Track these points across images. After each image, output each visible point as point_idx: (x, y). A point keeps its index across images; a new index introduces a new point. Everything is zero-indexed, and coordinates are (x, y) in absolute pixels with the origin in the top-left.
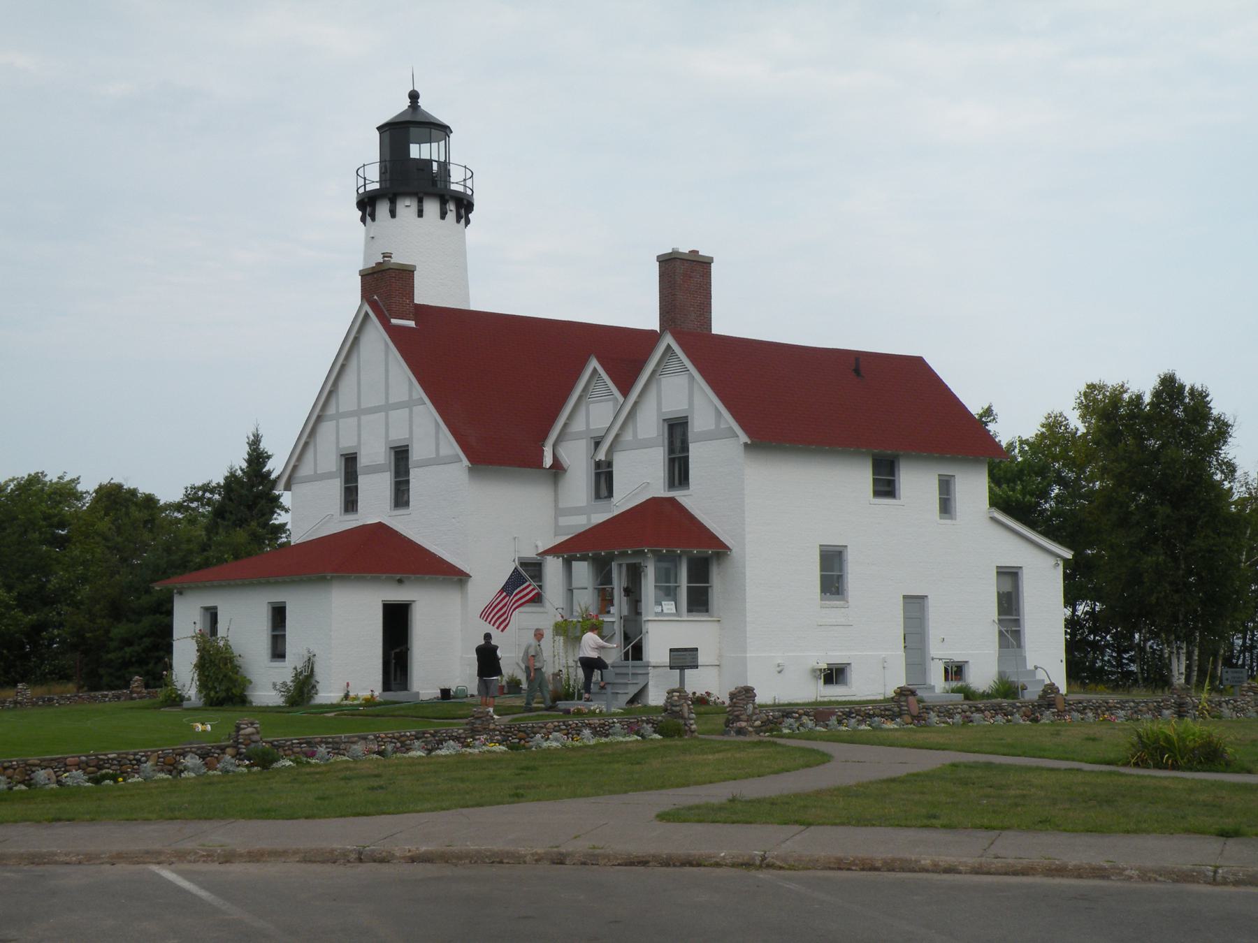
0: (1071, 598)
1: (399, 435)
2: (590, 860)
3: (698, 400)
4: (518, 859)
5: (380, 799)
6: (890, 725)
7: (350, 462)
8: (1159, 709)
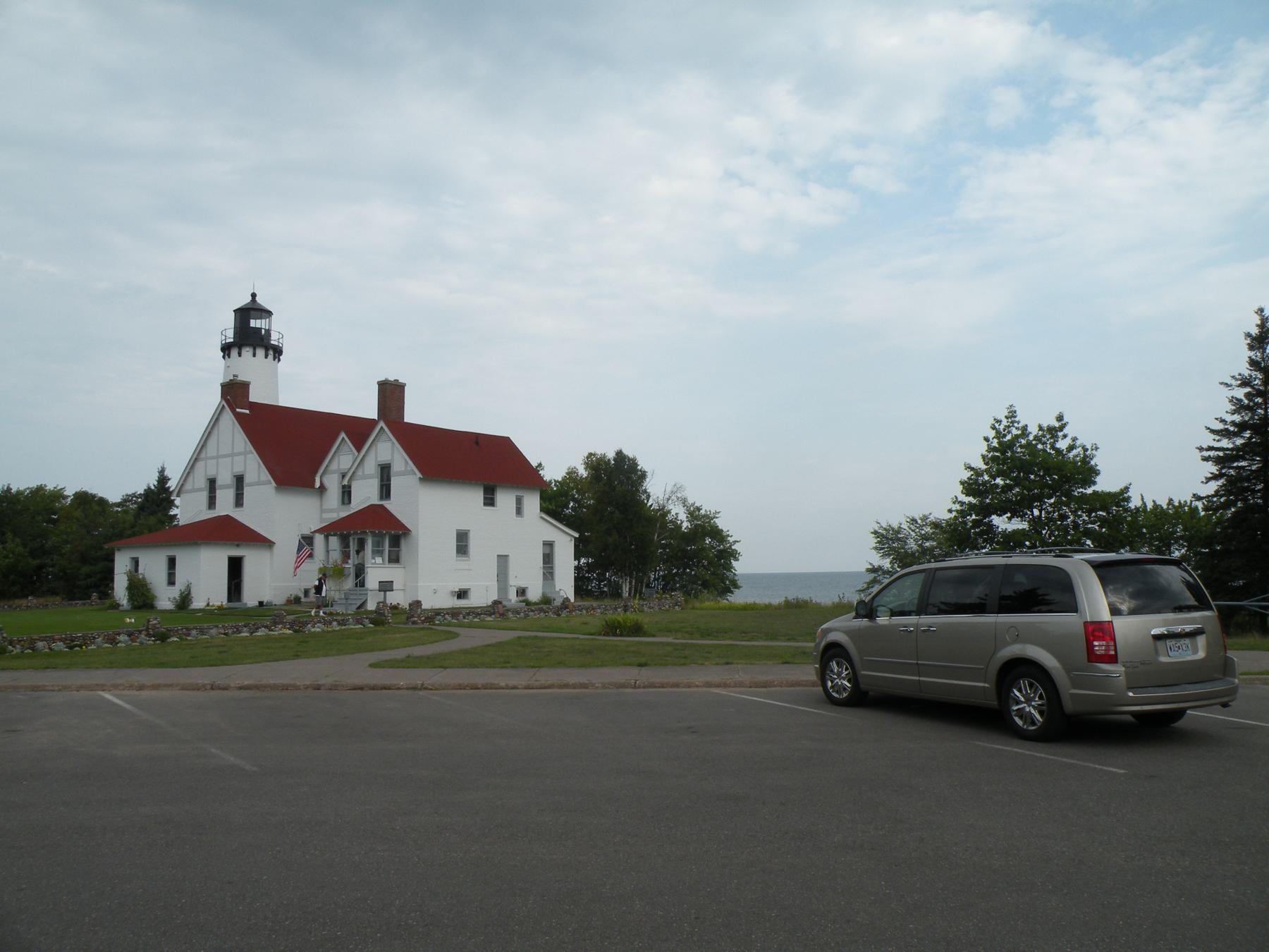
0: (577, 557)
1: (238, 470)
2: (334, 688)
3: (397, 456)
4: (297, 688)
5: (224, 657)
6: (489, 619)
7: (212, 483)
8: (616, 609)
